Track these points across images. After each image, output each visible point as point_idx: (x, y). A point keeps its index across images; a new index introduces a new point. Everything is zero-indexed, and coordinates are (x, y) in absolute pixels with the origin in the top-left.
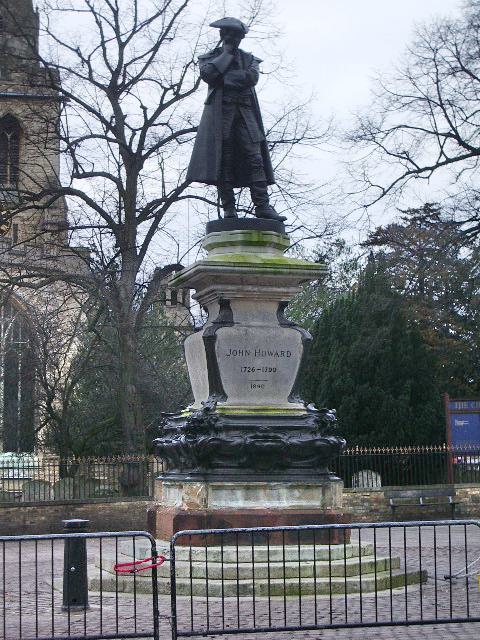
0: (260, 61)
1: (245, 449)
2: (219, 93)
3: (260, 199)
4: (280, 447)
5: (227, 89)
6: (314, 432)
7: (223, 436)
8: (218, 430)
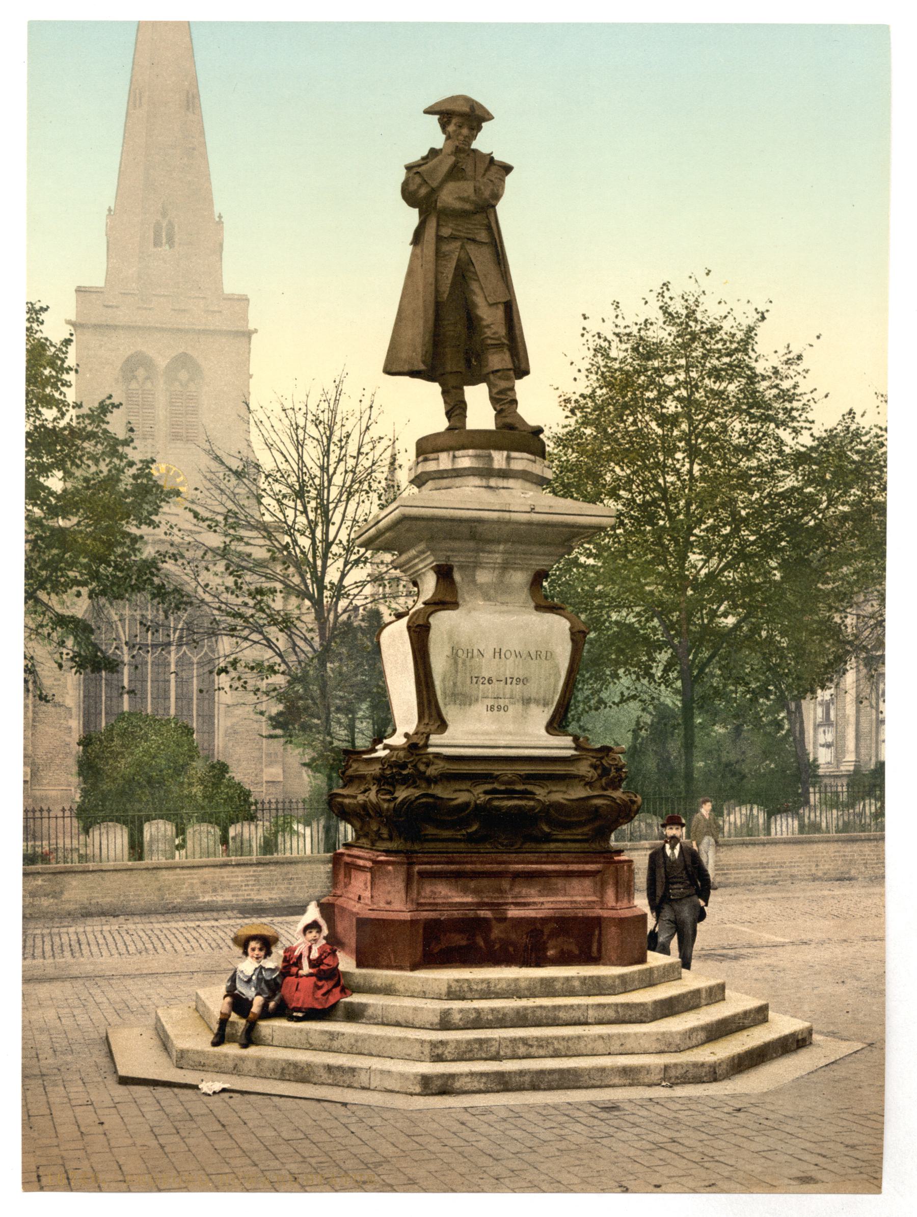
0: (508, 169)
1: (481, 812)
2: (432, 224)
3: (504, 402)
4: (533, 808)
5: (445, 214)
6: (590, 784)
7: (438, 791)
8: (430, 781)
